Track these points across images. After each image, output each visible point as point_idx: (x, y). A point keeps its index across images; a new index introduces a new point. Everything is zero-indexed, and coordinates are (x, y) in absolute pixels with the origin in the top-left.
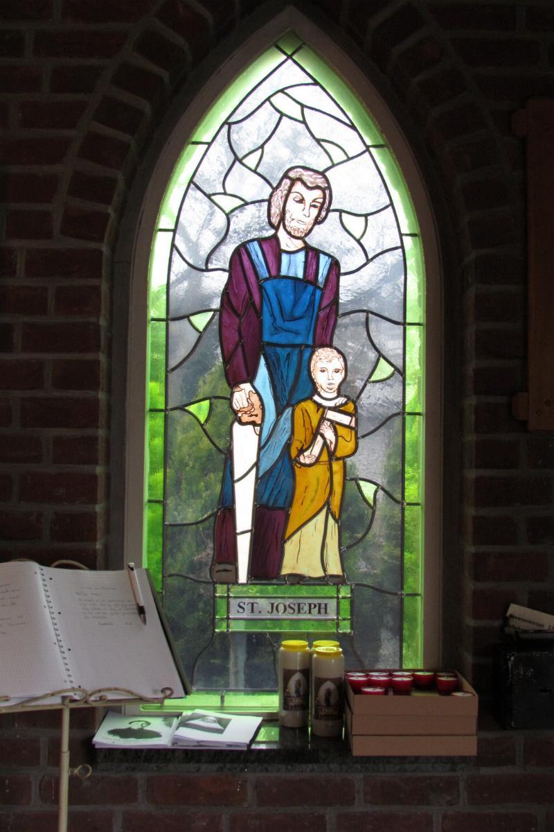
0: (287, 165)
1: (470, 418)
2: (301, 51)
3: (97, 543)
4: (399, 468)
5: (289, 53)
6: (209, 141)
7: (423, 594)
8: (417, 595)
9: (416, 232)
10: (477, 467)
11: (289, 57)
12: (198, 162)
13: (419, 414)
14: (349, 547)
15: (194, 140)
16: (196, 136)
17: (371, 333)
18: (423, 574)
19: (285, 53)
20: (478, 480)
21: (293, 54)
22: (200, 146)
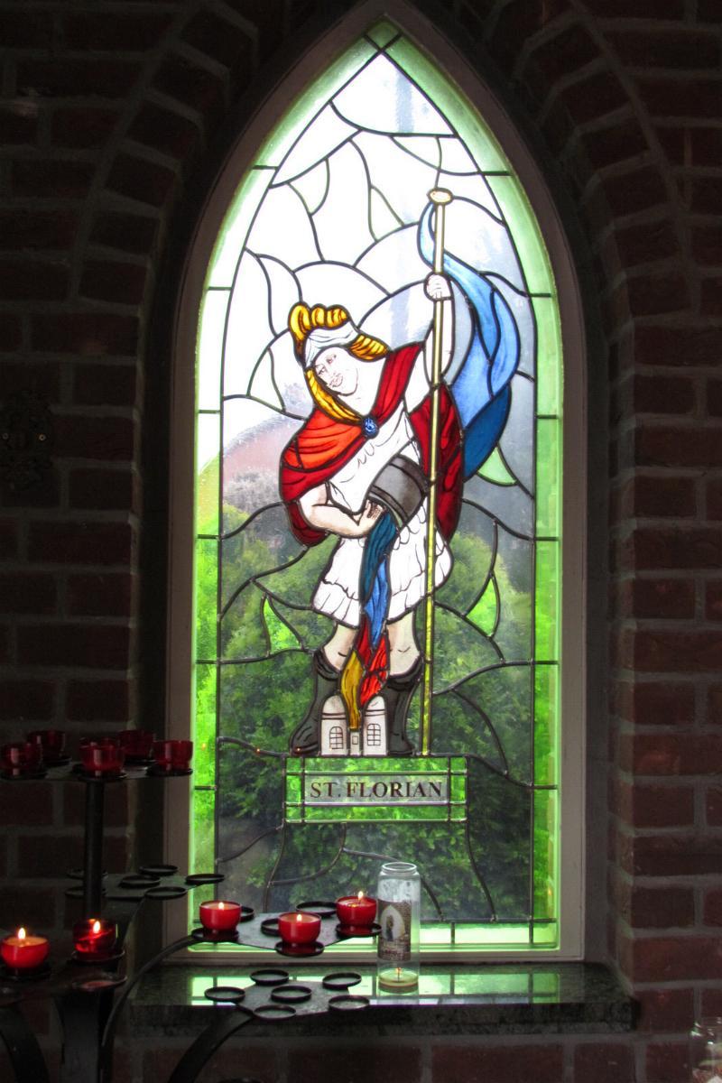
0: (370, 224)
1: (626, 500)
2: (397, 44)
3: (129, 671)
4: (530, 616)
5: (381, 45)
6: (277, 165)
7: (560, 787)
8: (552, 788)
9: (549, 291)
10: (637, 514)
11: (381, 51)
12: (248, 228)
13: (554, 417)
14: (458, 693)
15: (258, 163)
16: (261, 157)
17: (495, 330)
18: (561, 715)
19: (375, 45)
20: (639, 534)
21: (388, 45)
22: (265, 171)
